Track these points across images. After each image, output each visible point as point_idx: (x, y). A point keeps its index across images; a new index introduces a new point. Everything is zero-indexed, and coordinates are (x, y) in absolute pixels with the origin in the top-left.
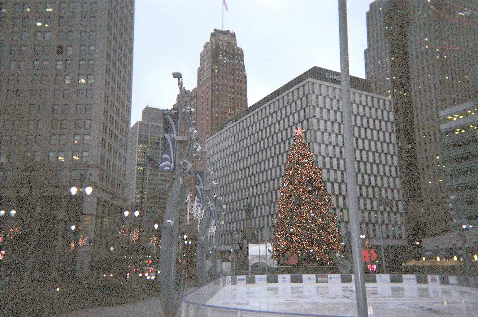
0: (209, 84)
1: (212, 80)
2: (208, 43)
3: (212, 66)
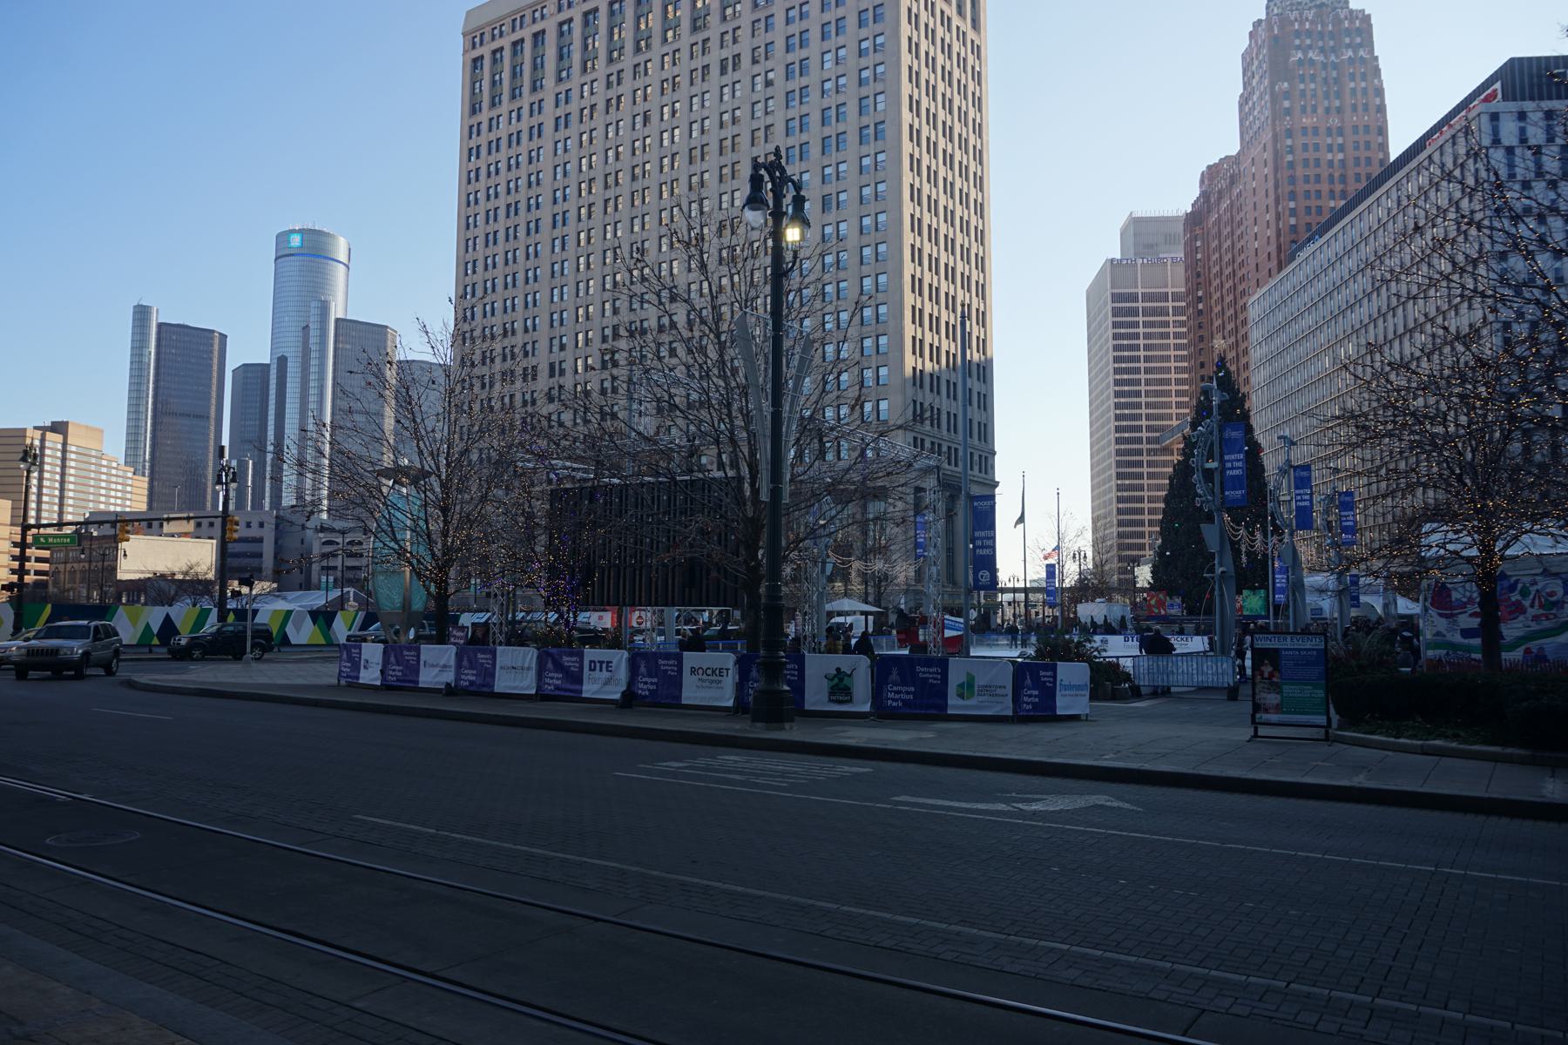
0: (1267, 137)
1: (1274, 125)
2: (1260, 21)
3: (1272, 84)
